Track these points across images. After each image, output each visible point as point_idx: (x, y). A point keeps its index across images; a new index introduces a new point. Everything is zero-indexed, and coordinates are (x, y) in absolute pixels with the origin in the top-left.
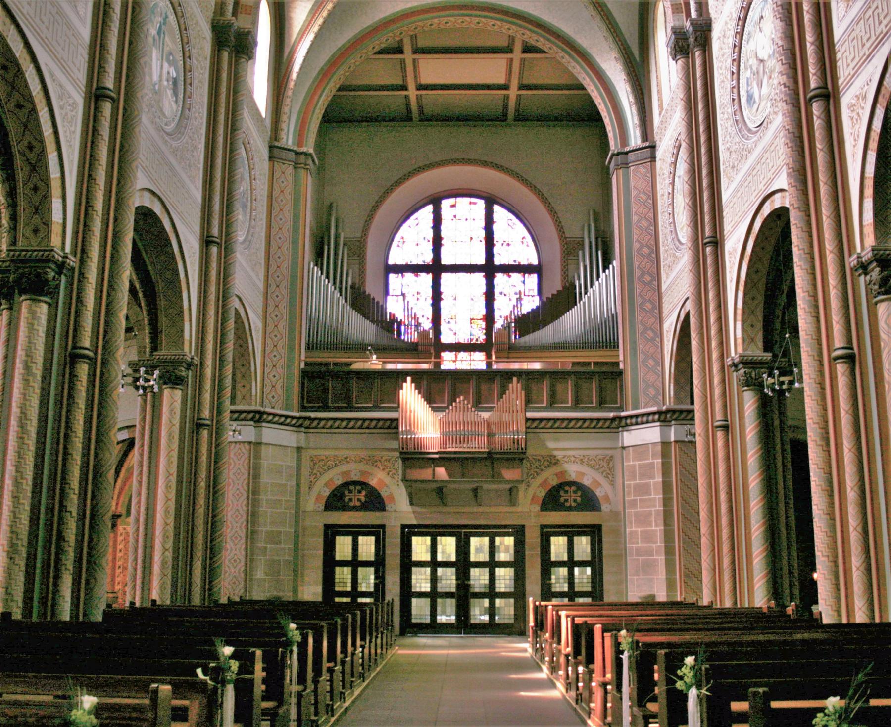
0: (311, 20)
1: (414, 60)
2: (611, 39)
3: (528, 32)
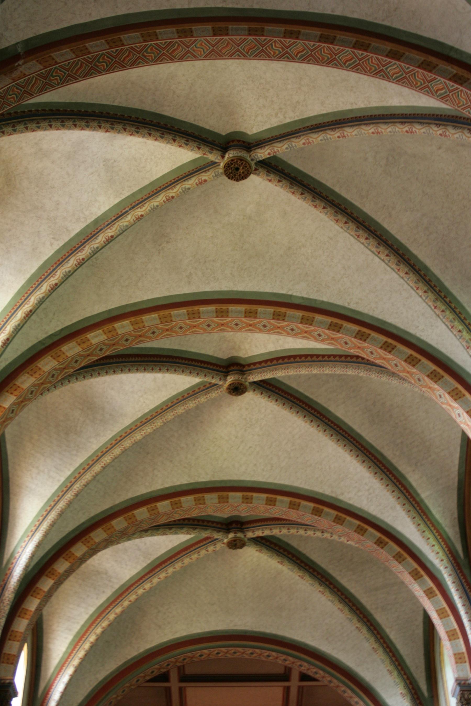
0: (72, 652)
1: (181, 689)
2: (395, 673)
3: (306, 664)
